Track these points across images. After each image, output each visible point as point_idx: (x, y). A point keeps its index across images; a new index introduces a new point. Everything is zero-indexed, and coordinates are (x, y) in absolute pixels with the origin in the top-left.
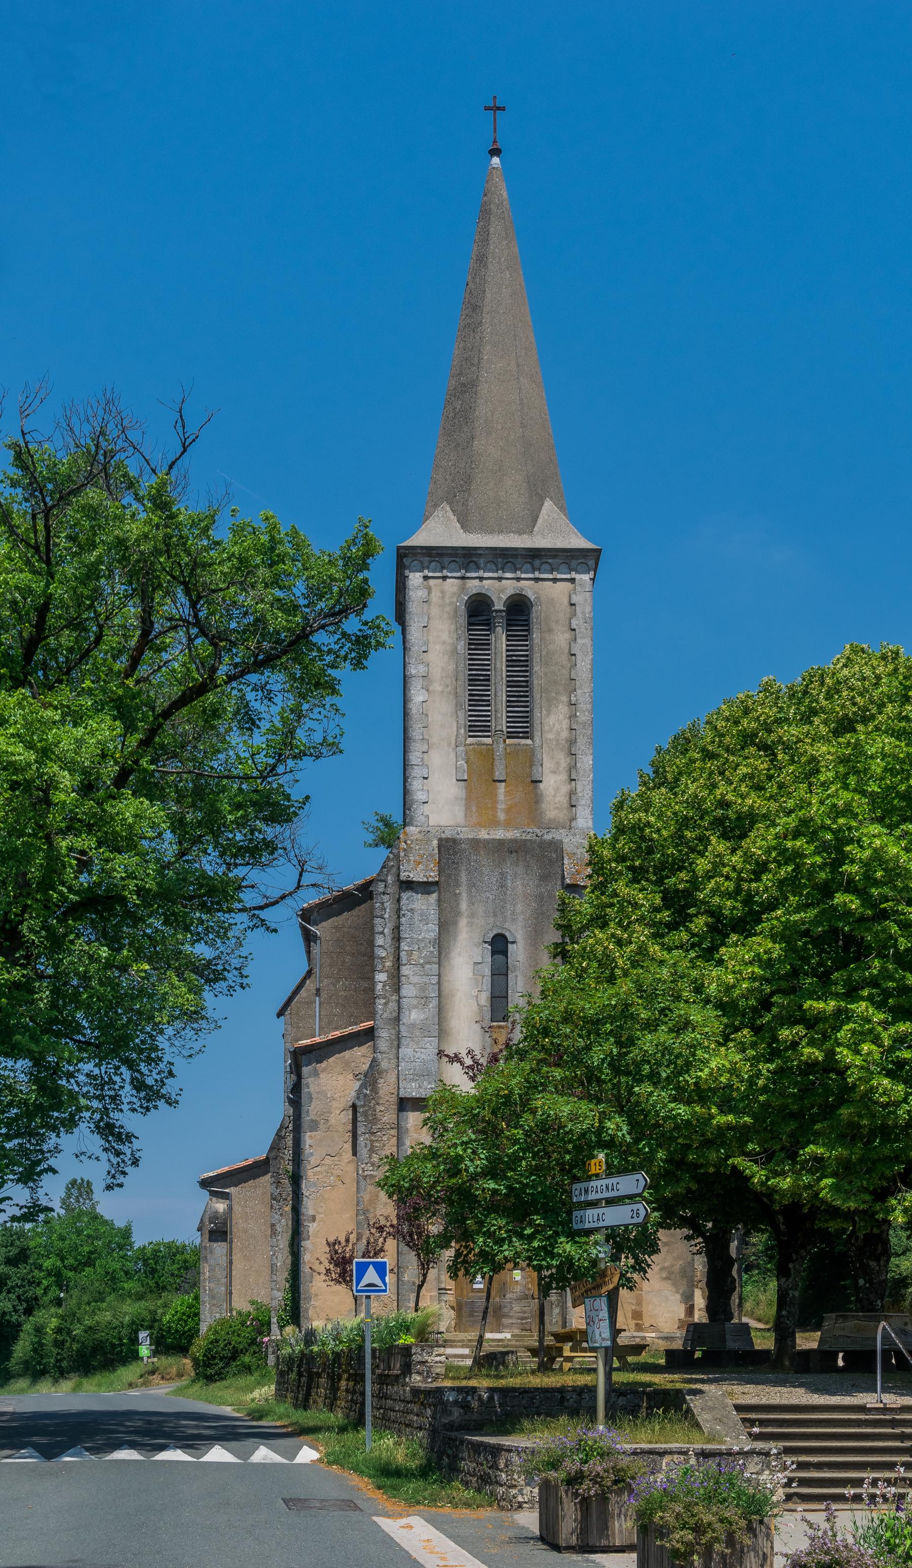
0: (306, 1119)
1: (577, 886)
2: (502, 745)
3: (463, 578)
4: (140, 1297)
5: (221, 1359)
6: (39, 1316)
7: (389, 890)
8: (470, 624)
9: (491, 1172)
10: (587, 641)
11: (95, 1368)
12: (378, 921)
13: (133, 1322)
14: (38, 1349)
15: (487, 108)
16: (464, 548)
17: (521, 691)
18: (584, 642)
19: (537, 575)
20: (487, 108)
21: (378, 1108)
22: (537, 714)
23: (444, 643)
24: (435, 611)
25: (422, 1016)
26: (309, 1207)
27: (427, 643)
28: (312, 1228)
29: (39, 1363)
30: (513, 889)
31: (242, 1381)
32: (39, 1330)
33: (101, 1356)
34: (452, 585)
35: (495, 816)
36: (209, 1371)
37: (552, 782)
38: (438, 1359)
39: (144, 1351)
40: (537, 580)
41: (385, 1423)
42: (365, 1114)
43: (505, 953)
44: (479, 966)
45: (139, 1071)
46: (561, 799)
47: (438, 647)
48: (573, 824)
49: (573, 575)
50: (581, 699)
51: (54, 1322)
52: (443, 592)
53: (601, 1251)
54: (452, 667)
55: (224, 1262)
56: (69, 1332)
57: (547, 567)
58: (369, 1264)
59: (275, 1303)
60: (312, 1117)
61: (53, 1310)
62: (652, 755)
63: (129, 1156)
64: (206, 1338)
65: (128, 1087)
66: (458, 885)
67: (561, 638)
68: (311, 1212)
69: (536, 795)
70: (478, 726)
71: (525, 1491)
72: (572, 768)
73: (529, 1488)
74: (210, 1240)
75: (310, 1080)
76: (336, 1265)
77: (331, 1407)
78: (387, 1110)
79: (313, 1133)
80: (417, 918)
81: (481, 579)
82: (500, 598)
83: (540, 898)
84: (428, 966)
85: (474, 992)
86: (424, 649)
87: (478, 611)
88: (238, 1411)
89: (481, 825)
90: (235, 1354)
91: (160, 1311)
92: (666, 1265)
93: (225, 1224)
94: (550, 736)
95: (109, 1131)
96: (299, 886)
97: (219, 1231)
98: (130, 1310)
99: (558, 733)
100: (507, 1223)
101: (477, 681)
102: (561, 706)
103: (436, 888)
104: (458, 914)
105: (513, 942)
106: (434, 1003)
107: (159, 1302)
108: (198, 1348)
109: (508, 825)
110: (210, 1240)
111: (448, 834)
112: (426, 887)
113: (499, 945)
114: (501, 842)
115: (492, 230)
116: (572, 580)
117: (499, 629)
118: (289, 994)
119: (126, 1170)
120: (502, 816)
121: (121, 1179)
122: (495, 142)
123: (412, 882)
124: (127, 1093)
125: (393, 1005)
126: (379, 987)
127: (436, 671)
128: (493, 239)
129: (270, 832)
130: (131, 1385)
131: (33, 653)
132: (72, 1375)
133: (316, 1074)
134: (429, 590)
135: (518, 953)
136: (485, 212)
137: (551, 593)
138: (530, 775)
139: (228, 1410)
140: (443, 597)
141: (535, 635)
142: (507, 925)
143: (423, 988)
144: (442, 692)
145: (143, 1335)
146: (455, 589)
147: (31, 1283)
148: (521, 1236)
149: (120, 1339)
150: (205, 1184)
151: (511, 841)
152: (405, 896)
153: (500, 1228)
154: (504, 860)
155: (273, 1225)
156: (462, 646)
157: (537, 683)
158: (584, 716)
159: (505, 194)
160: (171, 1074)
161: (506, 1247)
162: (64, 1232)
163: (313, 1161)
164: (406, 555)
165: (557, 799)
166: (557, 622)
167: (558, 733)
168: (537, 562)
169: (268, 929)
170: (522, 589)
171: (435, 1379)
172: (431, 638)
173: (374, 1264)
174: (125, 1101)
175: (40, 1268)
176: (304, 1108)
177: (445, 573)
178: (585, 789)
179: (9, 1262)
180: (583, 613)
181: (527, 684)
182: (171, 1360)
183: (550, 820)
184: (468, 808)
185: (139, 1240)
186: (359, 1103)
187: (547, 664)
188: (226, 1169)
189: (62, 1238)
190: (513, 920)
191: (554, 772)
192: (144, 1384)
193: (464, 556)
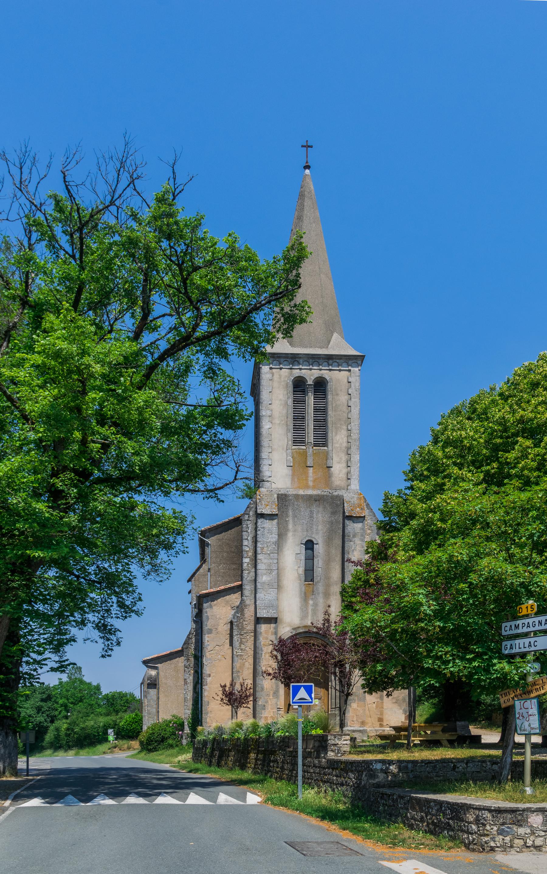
0: (205, 628)
1: (351, 516)
2: (311, 450)
3: (291, 369)
4: (107, 715)
5: (156, 742)
6: (57, 724)
7: (250, 519)
8: (294, 391)
9: (439, 614)
10: (357, 400)
11: (85, 745)
12: (244, 533)
13: (105, 726)
14: (57, 737)
15: (303, 146)
16: (291, 354)
17: (322, 424)
18: (355, 402)
19: (330, 367)
20: (303, 146)
21: (244, 623)
22: (330, 435)
23: (280, 400)
24: (276, 384)
25: (269, 579)
26: (207, 670)
27: (271, 400)
28: (208, 680)
29: (58, 743)
31: (170, 751)
32: (57, 729)
33: (88, 740)
34: (285, 372)
36: (149, 747)
38: (345, 742)
39: (111, 738)
40: (330, 370)
41: (308, 782)
42: (237, 626)
43: (312, 549)
45: (121, 598)
46: (343, 475)
47: (277, 402)
48: (349, 487)
49: (350, 368)
50: (353, 428)
51: (65, 726)
52: (280, 376)
53: (531, 668)
54: (285, 412)
55: (155, 698)
56: (73, 730)
57: (336, 364)
58: (301, 686)
59: (187, 716)
60: (209, 627)
61: (64, 721)
62: (474, 395)
63: (115, 640)
64: (147, 732)
65: (115, 605)
66: (287, 516)
67: (343, 398)
68: (208, 673)
69: (329, 474)
70: (299, 440)
71: (497, 839)
72: (348, 461)
73: (501, 837)
74: (148, 688)
75: (208, 610)
76: (226, 697)
77: (243, 767)
78: (249, 624)
80: (266, 531)
81: (301, 369)
82: (310, 379)
83: (331, 523)
84: (272, 555)
85: (296, 568)
87: (299, 385)
88: (174, 767)
89: (299, 488)
90: (163, 739)
91: (118, 721)
93: (155, 680)
94: (337, 445)
95: (105, 630)
96: (235, 479)
97: (153, 684)
98: (102, 720)
99: (341, 444)
100: (452, 650)
101: (298, 419)
104: (287, 530)
106: (275, 573)
107: (118, 717)
108: (143, 736)
109: (314, 488)
110: (148, 688)
111: (282, 492)
112: (271, 517)
113: (309, 545)
114: (310, 496)
115: (305, 204)
116: (349, 371)
117: (310, 394)
118: (194, 571)
119: (113, 648)
120: (311, 484)
121: (110, 652)
122: (307, 162)
123: (264, 514)
124: (115, 609)
125: (253, 574)
126: (245, 565)
127: (276, 414)
128: (306, 208)
129: (227, 434)
130: (104, 753)
131: (76, 297)
132: (74, 748)
133: (211, 607)
135: (319, 549)
136: (302, 196)
137: (337, 377)
139: (167, 767)
140: (280, 378)
141: (330, 397)
142: (313, 536)
143: (270, 565)
145: (110, 731)
146: (287, 374)
147: (53, 709)
148: (462, 659)
149: (98, 733)
150: (145, 662)
151: (316, 495)
152: (260, 521)
153: (446, 653)
155: (185, 679)
156: (290, 402)
157: (330, 419)
159: (312, 187)
160: (140, 599)
161: (451, 665)
162: (69, 688)
163: (209, 648)
165: (340, 476)
166: (341, 390)
167: (341, 444)
168: (331, 362)
169: (218, 499)
171: (343, 754)
172: (273, 398)
173: (304, 686)
174: (113, 612)
175: (57, 703)
176: (204, 623)
177: (281, 366)
178: (355, 471)
179: (42, 700)
180: (355, 386)
181: (325, 420)
182: (125, 742)
184: (293, 479)
185: (105, 691)
186: (234, 620)
187: (335, 411)
188: (156, 656)
189: (67, 691)
190: (317, 533)
191: (339, 463)
192: (111, 752)
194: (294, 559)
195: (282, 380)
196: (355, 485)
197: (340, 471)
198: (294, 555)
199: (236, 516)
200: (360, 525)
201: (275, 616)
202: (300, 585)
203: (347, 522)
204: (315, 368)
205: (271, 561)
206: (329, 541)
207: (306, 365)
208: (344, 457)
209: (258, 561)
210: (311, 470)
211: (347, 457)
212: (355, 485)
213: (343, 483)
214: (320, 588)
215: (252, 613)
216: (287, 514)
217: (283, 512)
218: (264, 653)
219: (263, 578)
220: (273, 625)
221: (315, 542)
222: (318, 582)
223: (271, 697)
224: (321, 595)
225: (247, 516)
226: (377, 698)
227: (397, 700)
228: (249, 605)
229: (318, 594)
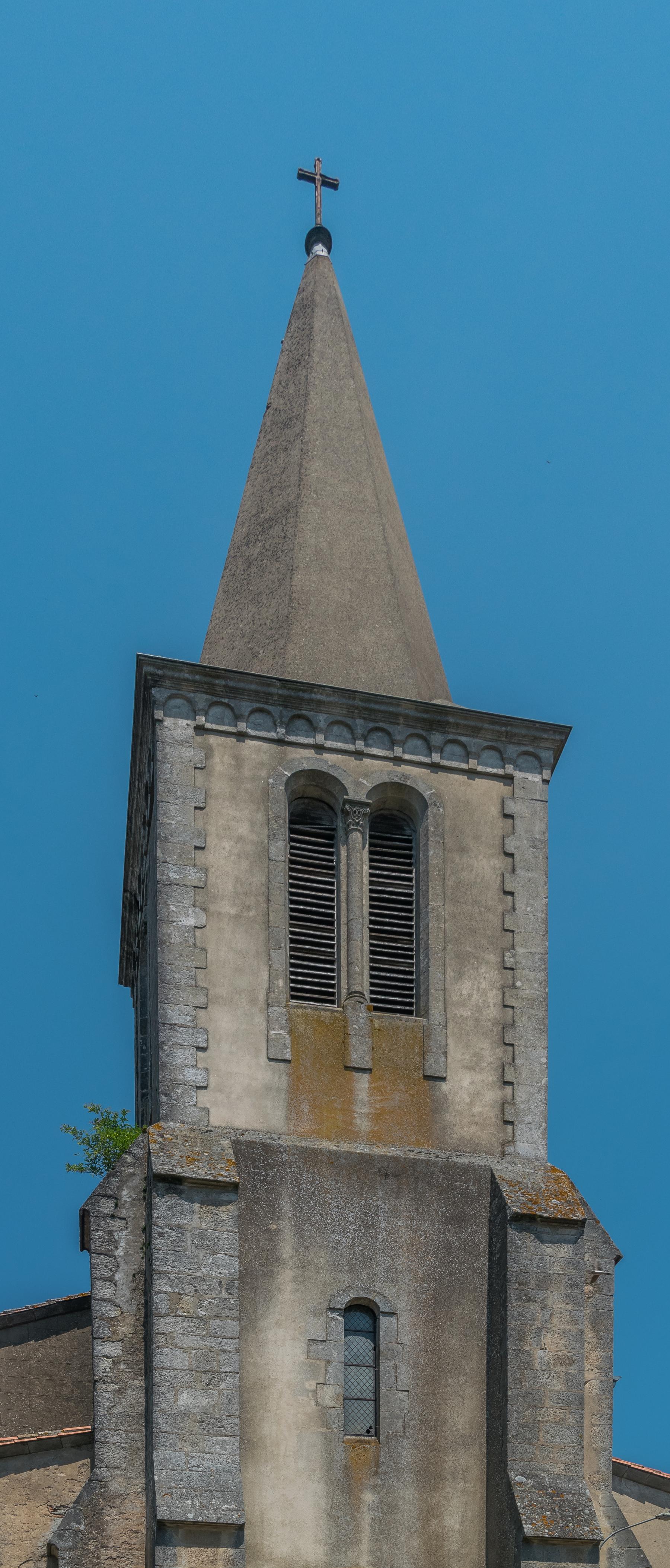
3: (280, 742)
21: (104, 1554)
23: (240, 839)
37: (466, 1083)
40: (435, 767)
43: (373, 1334)
44: (320, 1346)
48: (509, 1149)
49: (510, 769)
50: (524, 962)
54: (258, 879)
57: (457, 749)
66: (274, 1216)
81: (320, 748)
82: (358, 784)
84: (215, 1322)
85: (311, 1385)
86: (197, 842)
87: (312, 813)
89: (320, 1135)
99: (479, 1009)
102: (483, 969)
103: (232, 1197)
104: (273, 1261)
105: (391, 1314)
109: (375, 1138)
112: (212, 1191)
113: (362, 1315)
114: (365, 1161)
115: (317, 325)
117: (356, 837)
120: (363, 1125)
125: (135, 1395)
126: (104, 1365)
134: (209, 752)
135: (401, 1330)
137: (464, 800)
142: (377, 1287)
144: (237, 917)
158: (530, 986)
164: (157, 681)
165: (476, 1110)
166: (477, 838)
168: (437, 738)
170: (406, 777)
172: (212, 829)
178: (531, 1099)
183: (462, 1139)
186: (61, 1544)
191: (470, 1068)
194: (303, 1357)
195: (247, 773)
196: (530, 1143)
197: (476, 1096)
199: (75, 1295)
200: (565, 1251)
201: (234, 1518)
203: (514, 1236)
204: (375, 751)
205: (213, 1343)
206: (435, 1307)
207: (338, 738)
208: (490, 1054)
209: (159, 1340)
210: (363, 1082)
211: (499, 1052)
212: (530, 1143)
213: (488, 1135)
214: (407, 1454)
215: (137, 1507)
217: (257, 1201)
219: (182, 1399)
220: (224, 1553)
221: (384, 1307)
222: (396, 1434)
225: (111, 1203)
228: (123, 1497)
229: (398, 1472)
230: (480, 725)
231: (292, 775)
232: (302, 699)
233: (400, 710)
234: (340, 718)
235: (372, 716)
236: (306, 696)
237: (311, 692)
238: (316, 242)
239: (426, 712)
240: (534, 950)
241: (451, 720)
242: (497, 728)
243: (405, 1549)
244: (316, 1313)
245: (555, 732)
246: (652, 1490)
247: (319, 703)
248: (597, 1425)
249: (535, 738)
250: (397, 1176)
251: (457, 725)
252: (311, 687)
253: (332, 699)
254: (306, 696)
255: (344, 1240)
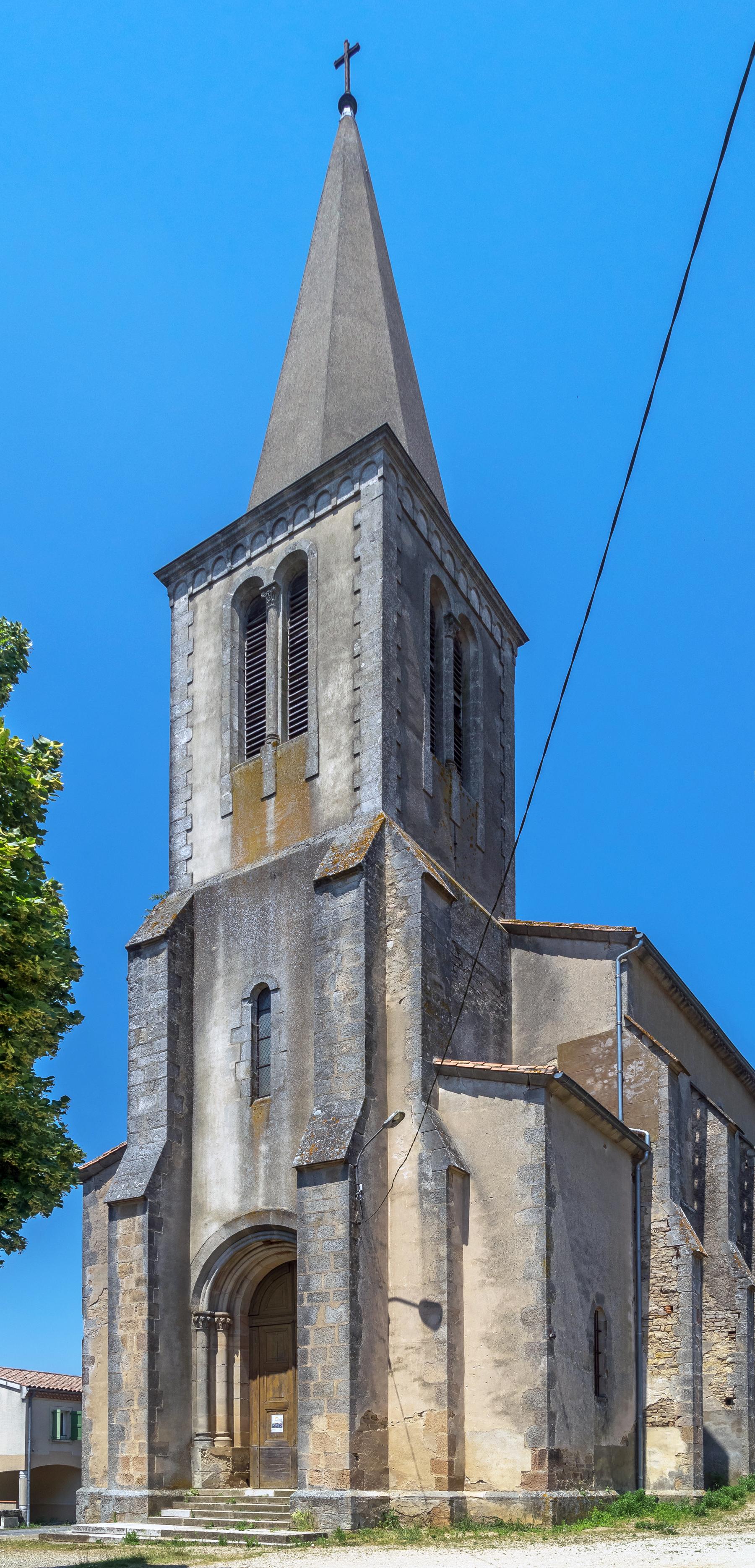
25: (150, 1105)
30: (276, 922)
35: (264, 843)
44: (238, 1032)
46: (344, 787)
66: (214, 940)
70: (253, 740)
79: (93, 1267)
82: (269, 571)
85: (232, 1066)
92: (501, 1393)
105: (277, 990)
113: (261, 998)
114: (263, 870)
138: (304, 774)
154: (266, 891)
193: (227, 543)
194: (228, 1045)
198: (227, 1035)
202: (241, 1110)
205: (154, 1059)
210: (272, 803)
216: (213, 935)
218: (122, 1291)
223: (136, 1407)
224: (286, 1124)
226: (428, 1400)
227: (509, 1405)
229: (280, 1121)
230: (331, 470)
231: (235, 593)
232: (234, 535)
233: (286, 498)
234: (257, 531)
235: (229, 542)
236: (235, 531)
237: (237, 526)
238: (346, 105)
239: (299, 487)
240: (371, 631)
241: (314, 480)
242: (342, 463)
243: (284, 1187)
244: (234, 1007)
245: (378, 435)
246: (484, 1083)
247: (243, 529)
248: (410, 1038)
249: (368, 450)
250: (280, 874)
251: (319, 481)
252: (235, 524)
253: (249, 522)
254: (235, 531)
255: (250, 941)
